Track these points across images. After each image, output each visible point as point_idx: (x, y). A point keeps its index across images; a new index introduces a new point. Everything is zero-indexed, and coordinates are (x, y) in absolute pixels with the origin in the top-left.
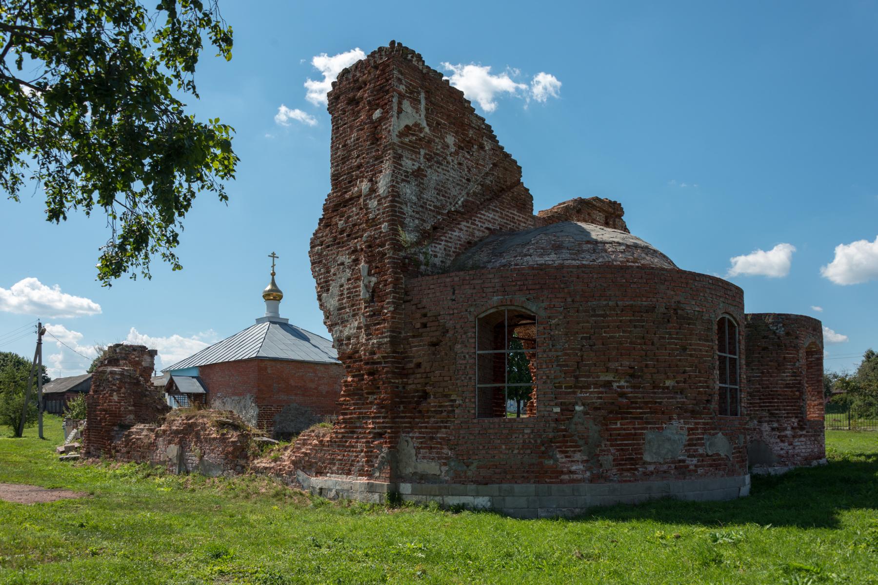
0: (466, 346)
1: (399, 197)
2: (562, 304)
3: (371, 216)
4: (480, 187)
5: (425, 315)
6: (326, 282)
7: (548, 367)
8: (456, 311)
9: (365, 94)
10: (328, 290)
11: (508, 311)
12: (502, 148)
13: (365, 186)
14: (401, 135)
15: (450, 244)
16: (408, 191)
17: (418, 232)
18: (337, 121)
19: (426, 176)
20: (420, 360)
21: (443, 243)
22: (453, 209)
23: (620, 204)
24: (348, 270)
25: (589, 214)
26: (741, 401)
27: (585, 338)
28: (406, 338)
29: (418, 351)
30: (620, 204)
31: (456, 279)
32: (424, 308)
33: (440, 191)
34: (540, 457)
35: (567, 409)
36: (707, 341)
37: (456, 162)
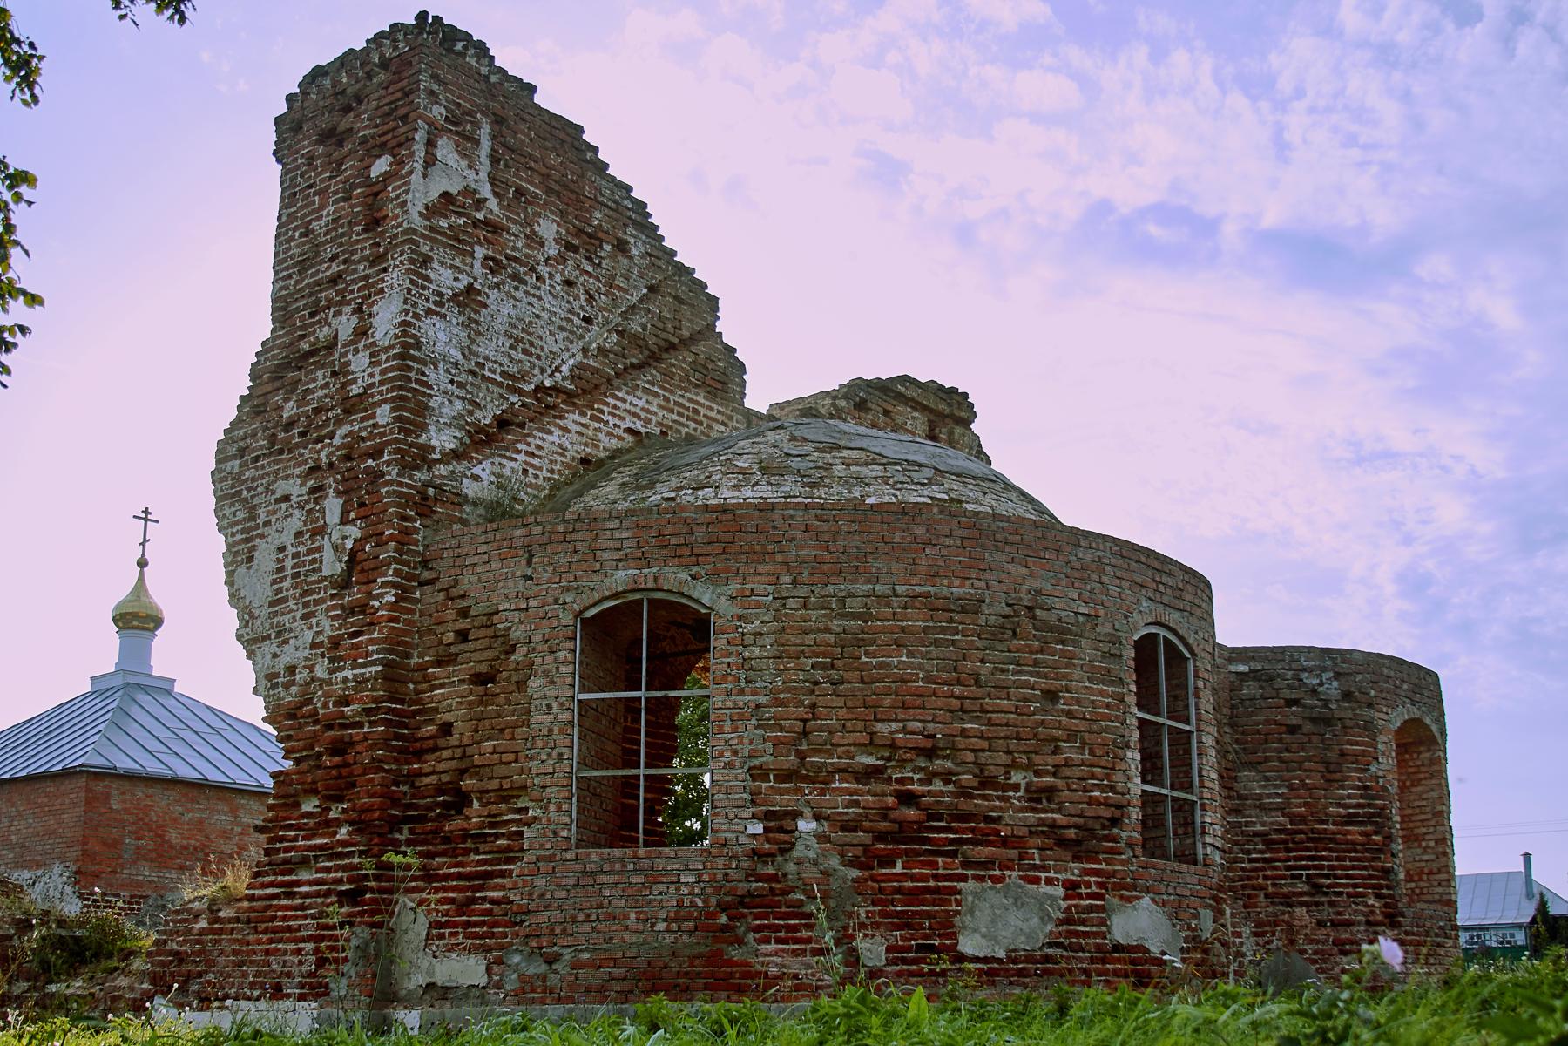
0: (553, 682)
1: (420, 349)
2: (771, 588)
3: (355, 390)
4: (615, 337)
5: (464, 613)
6: (247, 540)
7: (735, 730)
8: (533, 603)
9: (363, 124)
10: (250, 559)
11: (650, 601)
12: (673, 253)
13: (345, 324)
14: (431, 211)
15: (536, 462)
16: (442, 336)
17: (461, 428)
18: (293, 179)
19: (485, 306)
20: (448, 717)
21: (521, 457)
22: (547, 383)
23: (966, 395)
24: (297, 513)
25: (886, 413)
26: (1203, 833)
27: (824, 667)
28: (422, 668)
29: (450, 697)
30: (966, 395)
31: (537, 530)
32: (463, 597)
33: (518, 340)
34: (716, 940)
35: (779, 824)
36: (1112, 683)
37: (558, 278)
